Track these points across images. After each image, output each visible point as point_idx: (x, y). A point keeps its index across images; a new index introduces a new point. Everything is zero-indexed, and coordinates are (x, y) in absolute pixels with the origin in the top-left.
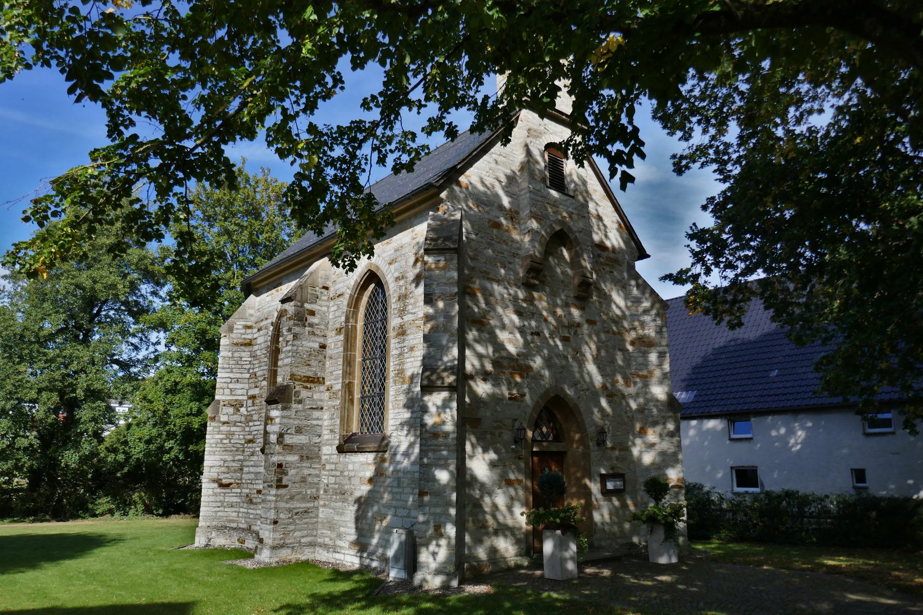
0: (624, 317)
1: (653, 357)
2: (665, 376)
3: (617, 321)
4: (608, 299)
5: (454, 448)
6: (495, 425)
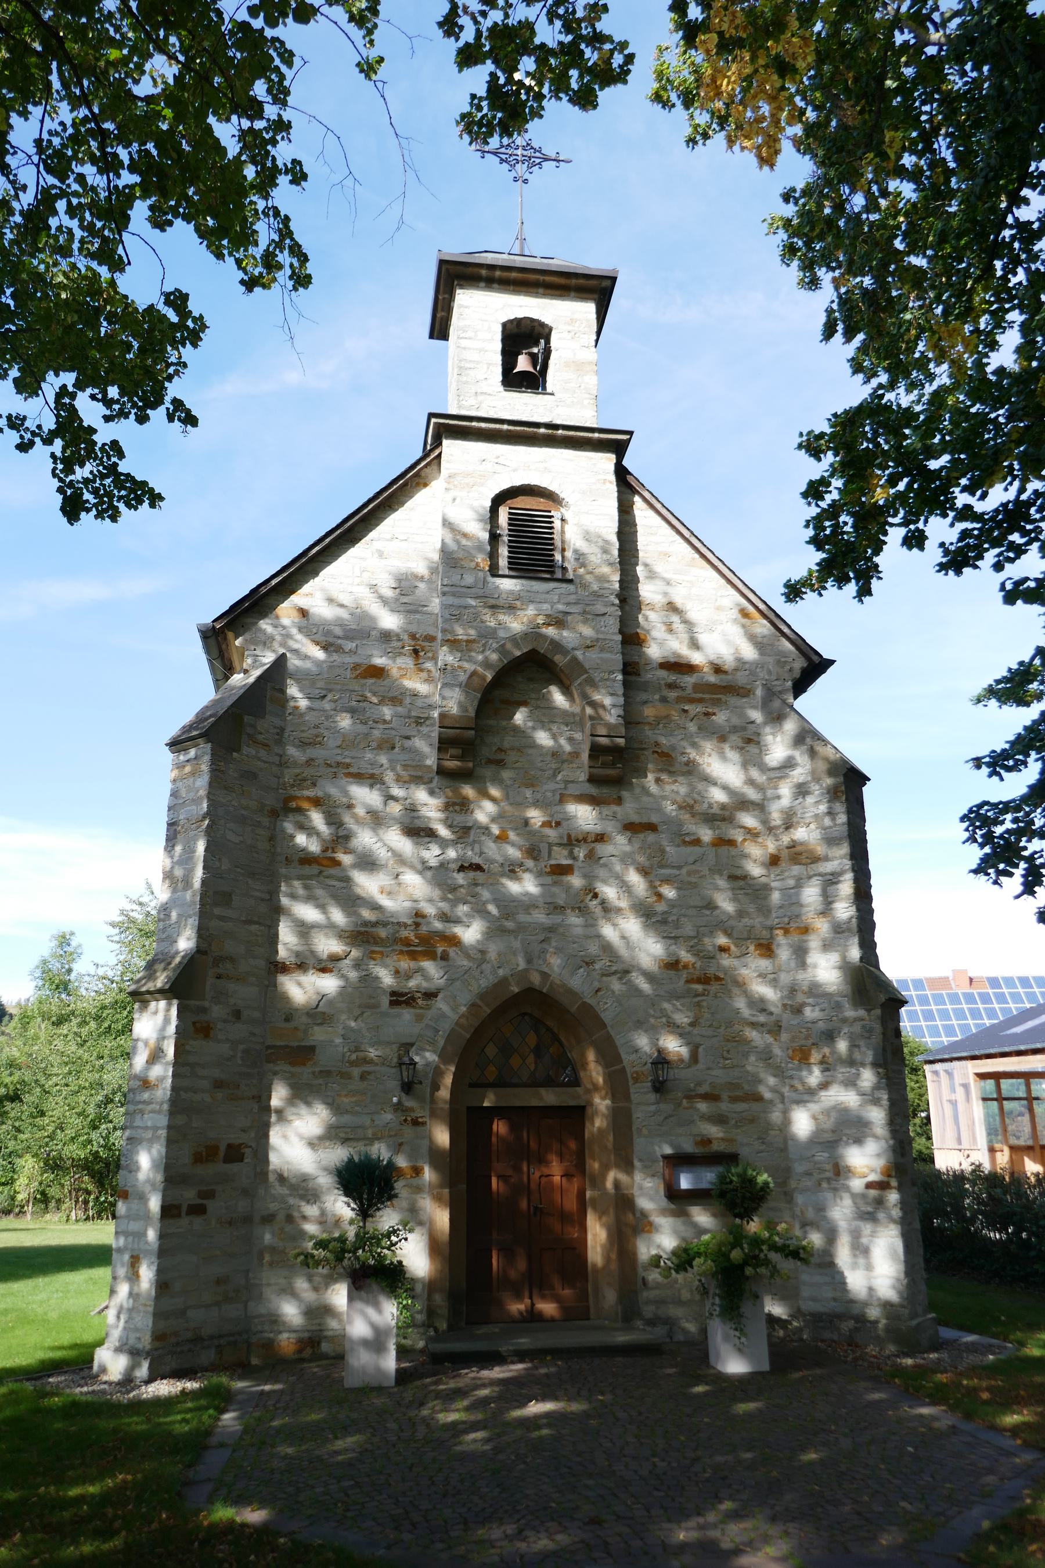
0: (743, 804)
1: (811, 894)
2: (839, 929)
3: (721, 817)
6: (354, 1057)
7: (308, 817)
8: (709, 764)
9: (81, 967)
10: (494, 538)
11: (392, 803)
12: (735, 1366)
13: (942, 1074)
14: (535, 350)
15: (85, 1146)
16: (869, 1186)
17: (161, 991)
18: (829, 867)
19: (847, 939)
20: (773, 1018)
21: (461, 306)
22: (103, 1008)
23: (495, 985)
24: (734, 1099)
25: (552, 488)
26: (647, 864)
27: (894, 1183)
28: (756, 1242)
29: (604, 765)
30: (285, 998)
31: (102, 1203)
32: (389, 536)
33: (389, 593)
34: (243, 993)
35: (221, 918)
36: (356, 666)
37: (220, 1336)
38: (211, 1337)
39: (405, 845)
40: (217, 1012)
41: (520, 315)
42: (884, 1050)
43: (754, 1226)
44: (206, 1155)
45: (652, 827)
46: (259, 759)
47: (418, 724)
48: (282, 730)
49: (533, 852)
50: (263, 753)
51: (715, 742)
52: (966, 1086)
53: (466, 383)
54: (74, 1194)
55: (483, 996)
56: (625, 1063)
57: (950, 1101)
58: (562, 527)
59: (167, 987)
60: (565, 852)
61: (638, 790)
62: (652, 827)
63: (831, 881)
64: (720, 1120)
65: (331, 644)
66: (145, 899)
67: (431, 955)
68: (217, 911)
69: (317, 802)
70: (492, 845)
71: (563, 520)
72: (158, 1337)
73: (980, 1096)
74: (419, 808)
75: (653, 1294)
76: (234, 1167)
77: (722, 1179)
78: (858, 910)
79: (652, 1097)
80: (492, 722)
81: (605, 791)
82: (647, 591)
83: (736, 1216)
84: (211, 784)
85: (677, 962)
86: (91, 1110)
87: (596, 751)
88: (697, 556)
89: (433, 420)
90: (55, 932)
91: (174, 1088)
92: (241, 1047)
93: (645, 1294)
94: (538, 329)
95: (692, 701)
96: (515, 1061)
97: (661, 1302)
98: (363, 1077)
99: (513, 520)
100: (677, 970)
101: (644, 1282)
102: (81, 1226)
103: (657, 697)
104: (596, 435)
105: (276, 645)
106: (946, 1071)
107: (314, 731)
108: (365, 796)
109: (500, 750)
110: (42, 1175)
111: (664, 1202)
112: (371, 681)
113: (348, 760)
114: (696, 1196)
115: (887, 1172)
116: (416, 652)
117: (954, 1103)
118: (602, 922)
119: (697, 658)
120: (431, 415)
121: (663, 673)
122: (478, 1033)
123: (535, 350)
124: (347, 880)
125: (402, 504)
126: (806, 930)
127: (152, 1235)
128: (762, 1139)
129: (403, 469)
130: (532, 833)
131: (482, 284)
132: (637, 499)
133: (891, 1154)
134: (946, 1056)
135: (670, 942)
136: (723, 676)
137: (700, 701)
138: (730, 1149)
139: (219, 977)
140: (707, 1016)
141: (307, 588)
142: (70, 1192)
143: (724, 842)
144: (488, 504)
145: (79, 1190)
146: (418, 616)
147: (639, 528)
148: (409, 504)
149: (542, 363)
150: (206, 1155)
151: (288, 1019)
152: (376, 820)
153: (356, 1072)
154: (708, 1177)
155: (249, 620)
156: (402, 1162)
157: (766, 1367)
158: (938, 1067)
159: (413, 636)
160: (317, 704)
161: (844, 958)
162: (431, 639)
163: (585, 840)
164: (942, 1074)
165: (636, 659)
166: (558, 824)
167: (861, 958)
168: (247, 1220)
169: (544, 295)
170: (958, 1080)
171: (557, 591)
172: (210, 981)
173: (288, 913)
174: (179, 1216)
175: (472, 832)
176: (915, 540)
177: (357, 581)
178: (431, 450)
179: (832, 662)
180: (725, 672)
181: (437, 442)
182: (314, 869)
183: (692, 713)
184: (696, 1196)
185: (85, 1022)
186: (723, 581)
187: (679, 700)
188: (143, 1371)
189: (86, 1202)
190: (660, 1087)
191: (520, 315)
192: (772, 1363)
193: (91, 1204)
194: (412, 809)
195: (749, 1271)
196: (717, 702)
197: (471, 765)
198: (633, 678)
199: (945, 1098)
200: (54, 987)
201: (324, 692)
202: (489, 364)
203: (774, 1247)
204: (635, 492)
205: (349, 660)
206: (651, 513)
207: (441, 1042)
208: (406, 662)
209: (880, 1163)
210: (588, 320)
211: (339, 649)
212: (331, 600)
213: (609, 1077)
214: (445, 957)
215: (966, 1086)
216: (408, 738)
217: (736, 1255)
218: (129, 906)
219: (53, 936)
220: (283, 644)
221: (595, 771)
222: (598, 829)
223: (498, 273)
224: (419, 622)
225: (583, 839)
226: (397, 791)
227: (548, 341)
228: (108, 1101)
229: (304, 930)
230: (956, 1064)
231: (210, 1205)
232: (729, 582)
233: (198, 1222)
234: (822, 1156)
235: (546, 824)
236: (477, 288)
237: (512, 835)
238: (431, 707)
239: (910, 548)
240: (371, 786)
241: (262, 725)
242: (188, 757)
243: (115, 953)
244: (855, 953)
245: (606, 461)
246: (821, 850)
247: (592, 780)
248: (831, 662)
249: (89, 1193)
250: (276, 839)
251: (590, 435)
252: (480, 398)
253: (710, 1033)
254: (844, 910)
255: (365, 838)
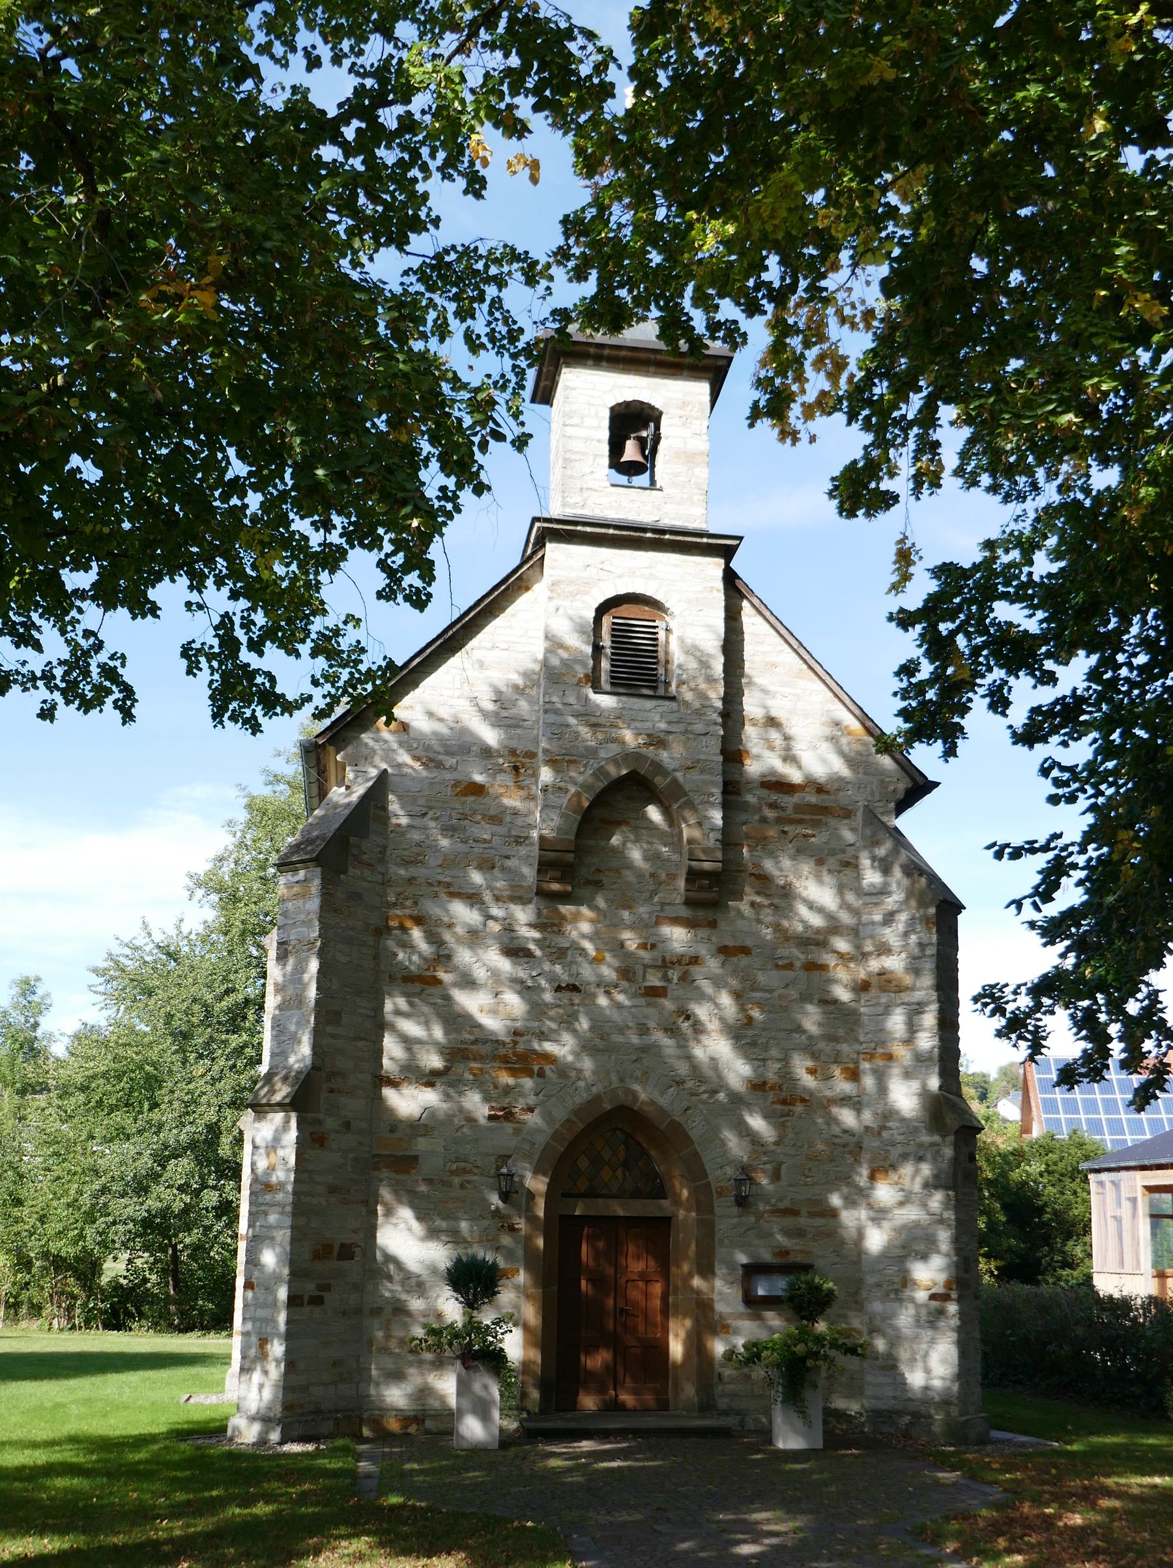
0: (834, 927)
1: (897, 1022)
2: (920, 1059)
3: (816, 941)
4: (784, 896)
5: (289, 1209)
6: (454, 1167)
7: (410, 936)
8: (806, 888)
9: (48, 1024)
10: (597, 649)
11: (491, 923)
12: (788, 1440)
13: (1108, 1185)
14: (644, 434)
15: (76, 1243)
16: (933, 1297)
17: (279, 1104)
18: (918, 995)
19: (927, 1067)
20: (854, 1140)
21: (567, 388)
22: (94, 1077)
23: (589, 1102)
24: (812, 1215)
25: (658, 597)
26: (739, 987)
27: (954, 1295)
28: (819, 1339)
29: (701, 889)
30: (391, 1112)
31: (90, 1310)
32: (489, 645)
33: (490, 706)
34: (353, 1106)
35: (333, 1036)
36: (457, 783)
37: (337, 1411)
38: (330, 1411)
39: (505, 965)
40: (331, 1123)
41: (629, 398)
42: (955, 1174)
43: (821, 1327)
44: (323, 1252)
45: (745, 951)
46: (364, 879)
47: (518, 843)
48: (385, 848)
49: (626, 973)
50: (367, 873)
51: (812, 864)
52: (1134, 1201)
53: (571, 477)
54: (56, 1298)
55: (578, 1112)
56: (711, 1178)
57: (1115, 1217)
58: (667, 638)
59: (287, 1101)
60: (660, 975)
61: (733, 913)
62: (745, 951)
63: (916, 1010)
64: (799, 1233)
65: (431, 760)
66: (139, 942)
67: (529, 1073)
68: (329, 1029)
69: (419, 921)
70: (586, 965)
71: (668, 630)
72: (287, 1407)
73: (1147, 1212)
74: (517, 928)
75: (729, 1388)
76: (346, 1264)
77: (792, 1286)
78: (941, 1039)
79: (735, 1210)
80: (591, 842)
81: (701, 914)
82: (751, 705)
83: (803, 1318)
84: (322, 908)
85: (765, 1083)
86: (86, 1201)
87: (693, 876)
88: (805, 667)
89: (537, 525)
90: (17, 977)
91: (295, 1193)
92: (352, 1155)
93: (720, 1388)
94: (647, 410)
95: (792, 822)
96: (606, 1174)
97: (733, 1396)
98: (462, 1186)
99: (616, 631)
100: (764, 1091)
101: (720, 1376)
102: (66, 1335)
103: (757, 817)
104: (705, 540)
105: (377, 760)
106: (1113, 1182)
107: (417, 850)
108: (463, 913)
109: (598, 870)
110: (15, 1275)
111: (741, 1308)
112: (472, 798)
113: (448, 879)
114: (770, 1302)
115: (948, 1285)
116: (516, 769)
117: (1118, 1220)
118: (692, 1043)
119: (796, 777)
120: (535, 519)
121: (764, 792)
122: (572, 1145)
123: (644, 434)
124: (448, 998)
125: (503, 610)
126: (890, 1057)
127: (282, 1318)
128: (837, 1253)
129: (504, 575)
130: (629, 955)
131: (590, 362)
132: (745, 603)
133: (953, 1269)
134: (1113, 1165)
135: (758, 1063)
136: (825, 797)
137: (800, 822)
138: (807, 1261)
139: (331, 1091)
140: (790, 1136)
141: (407, 700)
142: (51, 1296)
143: (815, 967)
144: (591, 615)
145: (62, 1293)
146: (518, 731)
147: (746, 636)
148: (510, 610)
149: (650, 449)
150: (323, 1252)
151: (393, 1130)
152: (475, 937)
153: (457, 1180)
154: (779, 1285)
155: (351, 734)
156: (502, 1264)
157: (820, 1445)
158: (1105, 1177)
159: (513, 752)
160: (418, 822)
161: (924, 1086)
162: (532, 755)
163: (679, 962)
164: (1108, 1185)
165: (737, 777)
166: (653, 946)
167: (941, 1088)
168: (358, 1311)
169: (655, 374)
170: (1125, 1193)
171: (660, 709)
172: (324, 1095)
173: (393, 1028)
174: (302, 1305)
175: (570, 952)
176: (999, 702)
177: (457, 693)
178: (534, 553)
179: (936, 784)
180: (828, 792)
181: (540, 544)
182: (417, 987)
183: (791, 835)
184: (770, 1302)
185: (66, 1093)
186: (830, 694)
187: (779, 821)
188: (275, 1436)
189: (70, 1308)
190: (742, 1202)
191: (629, 399)
192: (825, 1441)
193: (78, 1311)
194: (509, 928)
195: (810, 1363)
196: (816, 824)
197: (569, 888)
198: (732, 798)
199: (1109, 1214)
200: (17, 1046)
201: (425, 810)
202: (596, 456)
203: (834, 1345)
204: (743, 597)
205: (448, 776)
206: (759, 619)
207: (536, 1157)
208: (507, 779)
209: (942, 1277)
210: (701, 403)
211: (439, 765)
212: (431, 714)
213: (694, 1192)
214: (541, 1074)
215: (1134, 1201)
216: (508, 857)
217: (800, 1348)
218: (117, 950)
219: (14, 982)
220: (386, 759)
221: (691, 894)
222: (692, 952)
223: (606, 352)
224: (519, 737)
225: (679, 961)
226: (496, 911)
227: (657, 428)
228: (104, 1190)
229: (408, 1042)
230: (1123, 1174)
231: (326, 1296)
232: (836, 696)
233: (317, 1312)
234: (892, 1270)
235: (643, 946)
236: (585, 366)
237: (608, 957)
238: (531, 826)
239: (996, 712)
240: (472, 906)
241: (366, 845)
242: (297, 878)
243: (98, 1007)
244: (934, 1083)
245: (714, 567)
246: (908, 980)
247: (688, 902)
248: (936, 784)
249: (75, 1297)
250: (379, 956)
251: (698, 540)
252: (586, 494)
253: (793, 1152)
254: (927, 1041)
255: (464, 956)
